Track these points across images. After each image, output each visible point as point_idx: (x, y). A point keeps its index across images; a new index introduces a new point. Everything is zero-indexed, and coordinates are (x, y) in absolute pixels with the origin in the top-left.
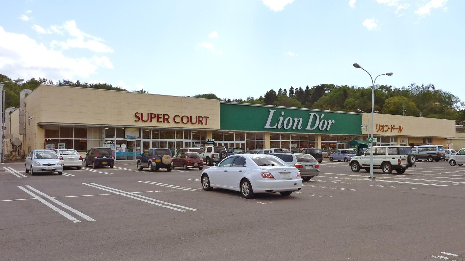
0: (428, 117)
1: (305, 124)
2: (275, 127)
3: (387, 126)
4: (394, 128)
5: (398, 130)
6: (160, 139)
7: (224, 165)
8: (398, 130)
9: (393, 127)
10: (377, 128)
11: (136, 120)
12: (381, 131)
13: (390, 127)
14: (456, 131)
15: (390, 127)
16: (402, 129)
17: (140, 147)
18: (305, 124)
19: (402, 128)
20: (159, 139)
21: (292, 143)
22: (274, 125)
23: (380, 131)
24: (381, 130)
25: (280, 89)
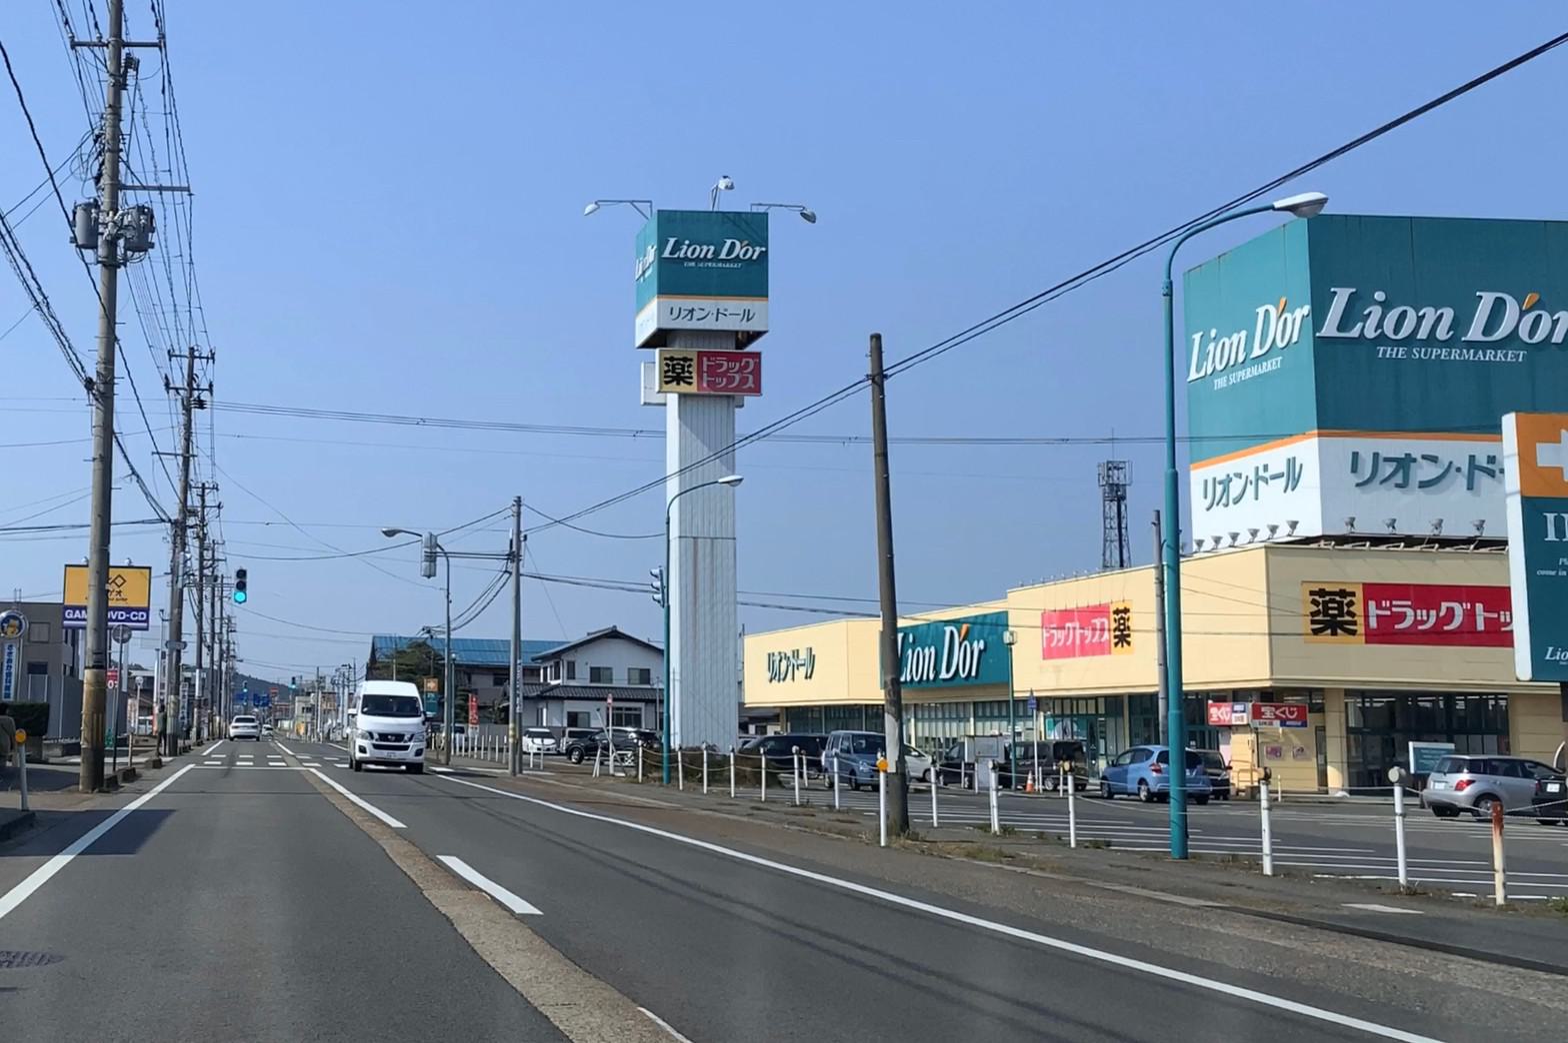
0: (684, 427)
1: (1460, 324)
2: (676, 256)
3: (1239, 476)
4: (1267, 475)
5: (1283, 480)
6: (1494, 894)
7: (789, 724)
8: (1283, 480)
9: (1261, 473)
10: (1206, 497)
11: (1253, 496)
12: (1221, 504)
13: (1252, 477)
14: (641, 670)
15: (1250, 479)
16: (1299, 476)
17: (1103, 712)
18: (1460, 324)
19: (1301, 466)
20: (1494, 885)
21: (636, 755)
22: (675, 253)
23: (1218, 504)
24: (1220, 500)
25: (1275, 524)
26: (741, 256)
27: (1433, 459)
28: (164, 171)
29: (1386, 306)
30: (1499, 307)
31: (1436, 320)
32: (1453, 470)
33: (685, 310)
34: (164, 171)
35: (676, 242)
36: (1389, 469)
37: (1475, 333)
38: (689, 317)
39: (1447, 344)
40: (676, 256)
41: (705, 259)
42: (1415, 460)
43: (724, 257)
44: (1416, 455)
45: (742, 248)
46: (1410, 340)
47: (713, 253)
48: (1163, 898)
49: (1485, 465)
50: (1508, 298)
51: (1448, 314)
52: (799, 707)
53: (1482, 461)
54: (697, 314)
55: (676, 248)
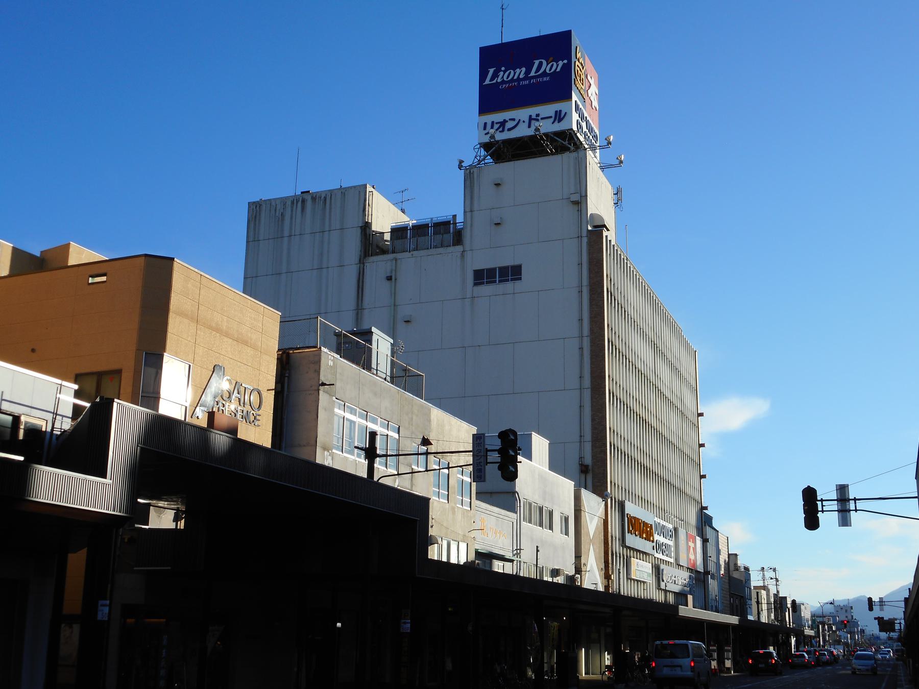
2: (495, 81)
6: (453, 245)
26: (548, 71)
27: (514, 120)
28: (443, 303)
29: (505, 72)
30: (540, 64)
31: (521, 72)
32: (521, 122)
33: (497, 123)
34: (443, 303)
35: (494, 71)
36: (496, 126)
37: (532, 74)
38: (501, 129)
39: (524, 79)
40: (495, 81)
41: (519, 79)
42: (507, 121)
43: (534, 74)
44: (507, 119)
45: (547, 65)
46: (512, 80)
47: (525, 73)
48: (329, 203)
49: (535, 118)
50: (542, 60)
51: (524, 69)
52: (436, 407)
53: (534, 117)
54: (509, 125)
55: (495, 75)
